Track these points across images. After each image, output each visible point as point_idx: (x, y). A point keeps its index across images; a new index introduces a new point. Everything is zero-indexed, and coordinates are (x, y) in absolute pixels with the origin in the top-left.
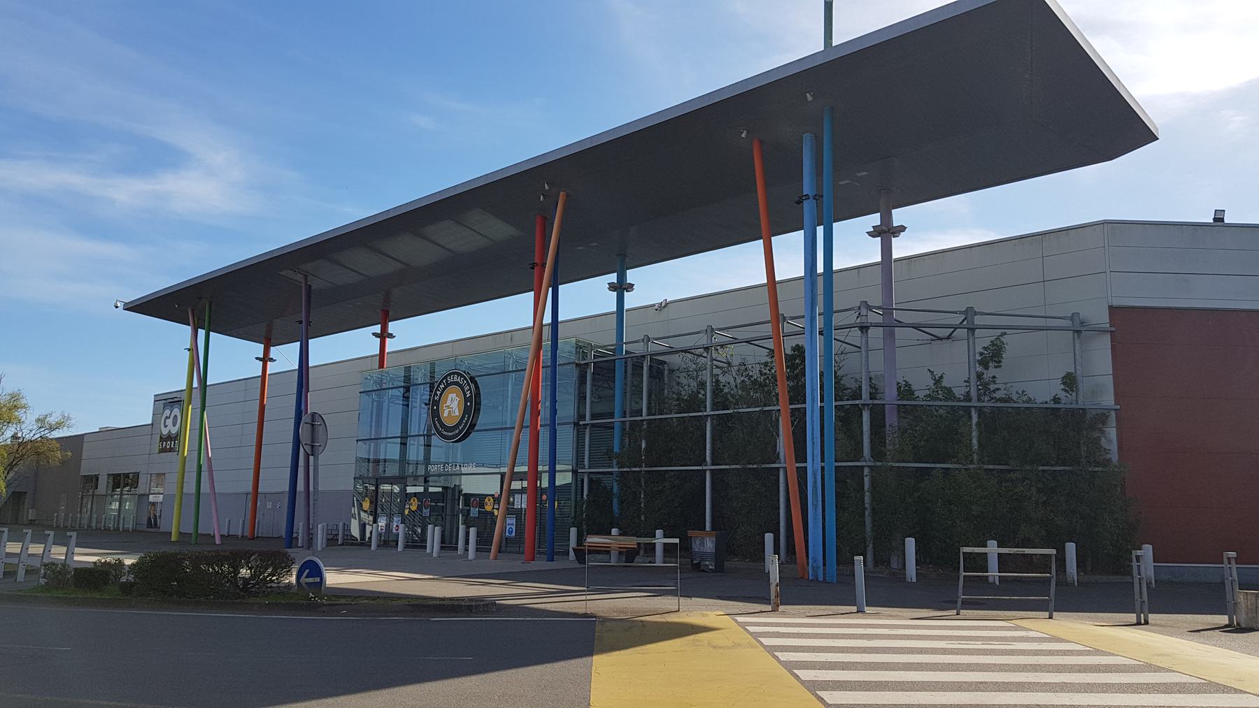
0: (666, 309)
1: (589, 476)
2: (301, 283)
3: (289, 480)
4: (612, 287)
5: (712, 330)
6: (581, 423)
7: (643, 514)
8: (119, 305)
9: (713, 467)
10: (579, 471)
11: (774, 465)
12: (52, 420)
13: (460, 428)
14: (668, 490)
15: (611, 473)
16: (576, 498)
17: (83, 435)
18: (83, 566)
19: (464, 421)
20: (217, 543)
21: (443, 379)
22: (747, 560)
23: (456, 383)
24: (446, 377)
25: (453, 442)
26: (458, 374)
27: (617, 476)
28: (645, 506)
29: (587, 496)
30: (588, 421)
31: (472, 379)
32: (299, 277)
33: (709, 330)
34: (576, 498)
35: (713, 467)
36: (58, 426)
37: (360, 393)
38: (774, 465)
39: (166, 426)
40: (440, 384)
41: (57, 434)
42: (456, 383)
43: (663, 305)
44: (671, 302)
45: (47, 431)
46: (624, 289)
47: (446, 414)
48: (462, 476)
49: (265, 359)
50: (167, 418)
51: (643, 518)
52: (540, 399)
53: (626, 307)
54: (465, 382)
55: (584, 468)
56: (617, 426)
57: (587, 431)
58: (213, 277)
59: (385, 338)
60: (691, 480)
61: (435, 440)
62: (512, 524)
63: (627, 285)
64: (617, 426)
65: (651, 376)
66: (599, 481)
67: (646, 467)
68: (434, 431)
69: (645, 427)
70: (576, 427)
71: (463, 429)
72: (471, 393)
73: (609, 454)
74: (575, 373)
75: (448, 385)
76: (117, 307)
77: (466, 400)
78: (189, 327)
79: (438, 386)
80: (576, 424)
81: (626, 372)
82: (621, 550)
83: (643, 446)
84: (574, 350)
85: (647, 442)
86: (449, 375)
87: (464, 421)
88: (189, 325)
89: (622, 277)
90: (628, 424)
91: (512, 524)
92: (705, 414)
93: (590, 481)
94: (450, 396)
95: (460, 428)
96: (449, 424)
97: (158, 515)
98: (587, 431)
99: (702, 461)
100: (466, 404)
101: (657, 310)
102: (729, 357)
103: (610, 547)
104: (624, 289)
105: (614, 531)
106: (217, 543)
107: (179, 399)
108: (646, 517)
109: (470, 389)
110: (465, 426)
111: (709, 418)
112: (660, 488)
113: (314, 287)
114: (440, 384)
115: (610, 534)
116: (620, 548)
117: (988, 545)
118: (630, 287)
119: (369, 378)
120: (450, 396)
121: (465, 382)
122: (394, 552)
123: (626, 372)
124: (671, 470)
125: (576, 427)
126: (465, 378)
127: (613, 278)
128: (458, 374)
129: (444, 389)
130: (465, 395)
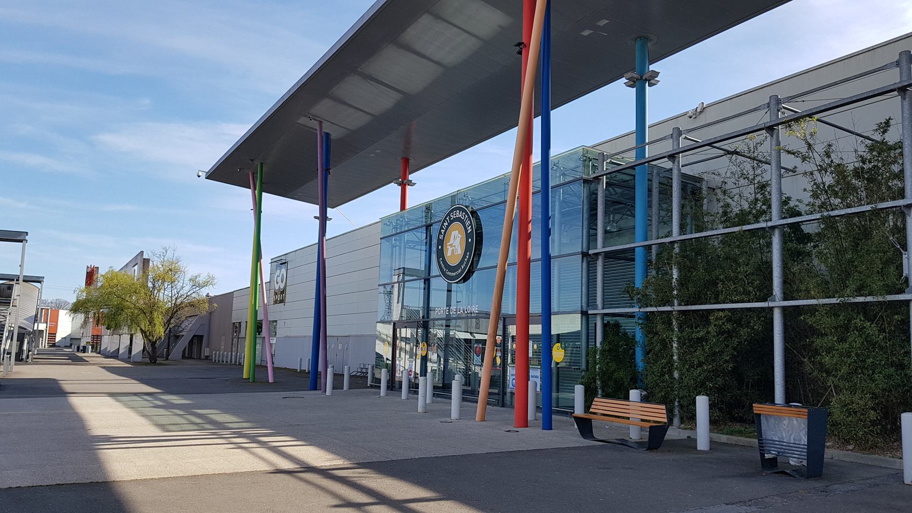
0: (703, 115)
1: (603, 319)
2: (316, 130)
3: (313, 327)
5: (778, 102)
6: (591, 252)
7: (676, 369)
8: (200, 174)
9: (787, 303)
10: (590, 312)
11: (901, 297)
12: (201, 280)
13: (463, 267)
14: (714, 336)
15: (631, 316)
16: (588, 347)
17: (233, 292)
20: (270, 382)
21: (446, 217)
22: (850, 447)
23: (458, 219)
24: (449, 215)
25: (457, 283)
26: (460, 209)
27: (639, 318)
28: (679, 358)
29: (601, 344)
30: (600, 248)
31: (474, 213)
32: (314, 124)
33: (773, 102)
34: (588, 347)
35: (787, 303)
36: (206, 284)
37: (381, 239)
38: (901, 297)
39: (277, 283)
41: (204, 292)
42: (458, 219)
43: (699, 110)
44: (709, 106)
45: (198, 289)
46: (646, 80)
47: (449, 254)
49: (323, 219)
50: (278, 276)
51: (676, 375)
52: (530, 218)
53: (648, 124)
54: (467, 217)
55: (596, 309)
56: (639, 255)
57: (600, 263)
59: (405, 185)
60: (749, 323)
62: (537, 377)
63: (650, 74)
64: (639, 255)
65: (683, 197)
66: (617, 326)
67: (680, 305)
69: (677, 250)
70: (585, 258)
71: (465, 268)
72: (472, 228)
73: (630, 291)
74: (581, 191)
76: (199, 176)
77: (468, 236)
78: (250, 190)
80: (585, 255)
83: (675, 274)
84: (580, 163)
85: (680, 270)
86: (452, 211)
88: (250, 189)
90: (654, 250)
91: (537, 377)
92: (770, 224)
93: (605, 326)
95: (463, 267)
97: (273, 353)
98: (600, 263)
99: (766, 294)
101: (691, 117)
102: (808, 137)
103: (628, 418)
104: (646, 80)
105: (634, 394)
106: (270, 382)
107: (285, 261)
108: (681, 375)
109: (471, 224)
110: (467, 265)
111: (777, 232)
112: (702, 334)
113: (334, 136)
115: (627, 398)
116: (642, 420)
119: (388, 224)
121: (467, 217)
122: (398, 399)
124: (719, 310)
125: (585, 258)
126: (467, 213)
128: (460, 209)
129: (448, 226)
130: (466, 230)
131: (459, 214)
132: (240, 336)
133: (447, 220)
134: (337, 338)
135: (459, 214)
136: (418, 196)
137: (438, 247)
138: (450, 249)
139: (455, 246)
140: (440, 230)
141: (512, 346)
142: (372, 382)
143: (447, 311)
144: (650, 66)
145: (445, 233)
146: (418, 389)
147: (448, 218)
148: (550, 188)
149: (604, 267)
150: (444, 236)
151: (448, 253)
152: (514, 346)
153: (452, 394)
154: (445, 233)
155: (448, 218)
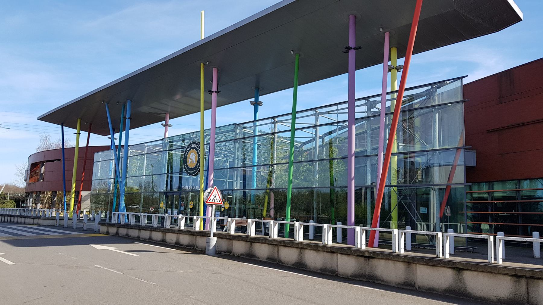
4: (252, 103)
13: (196, 169)
18: (104, 245)
19: (198, 166)
23: (194, 148)
26: (195, 143)
40: (187, 148)
42: (194, 148)
47: (189, 163)
48: (252, 190)
54: (198, 147)
58: (50, 113)
61: (185, 176)
68: (184, 170)
75: (191, 149)
79: (187, 149)
81: (533, 122)
82: (481, 233)
87: (198, 166)
89: (257, 99)
94: (191, 154)
95: (196, 169)
96: (191, 167)
100: (186, 159)
104: (258, 104)
114: (187, 148)
117: (448, 231)
118: (260, 104)
120: (191, 154)
121: (198, 147)
123: (533, 122)
127: (253, 100)
129: (189, 150)
131: (194, 146)
132: (127, 176)
133: (189, 148)
134: (62, 158)
135: (194, 146)
136: (172, 132)
137: (184, 159)
138: (190, 161)
139: (192, 159)
140: (185, 152)
141: (175, 203)
142: (265, 224)
143: (188, 188)
144: (415, 106)
145: (187, 153)
146: (309, 233)
147: (189, 147)
148: (291, 188)
149: (355, 160)
150: (187, 155)
151: (189, 162)
152: (176, 203)
153: (338, 236)
154: (187, 153)
155: (189, 147)
